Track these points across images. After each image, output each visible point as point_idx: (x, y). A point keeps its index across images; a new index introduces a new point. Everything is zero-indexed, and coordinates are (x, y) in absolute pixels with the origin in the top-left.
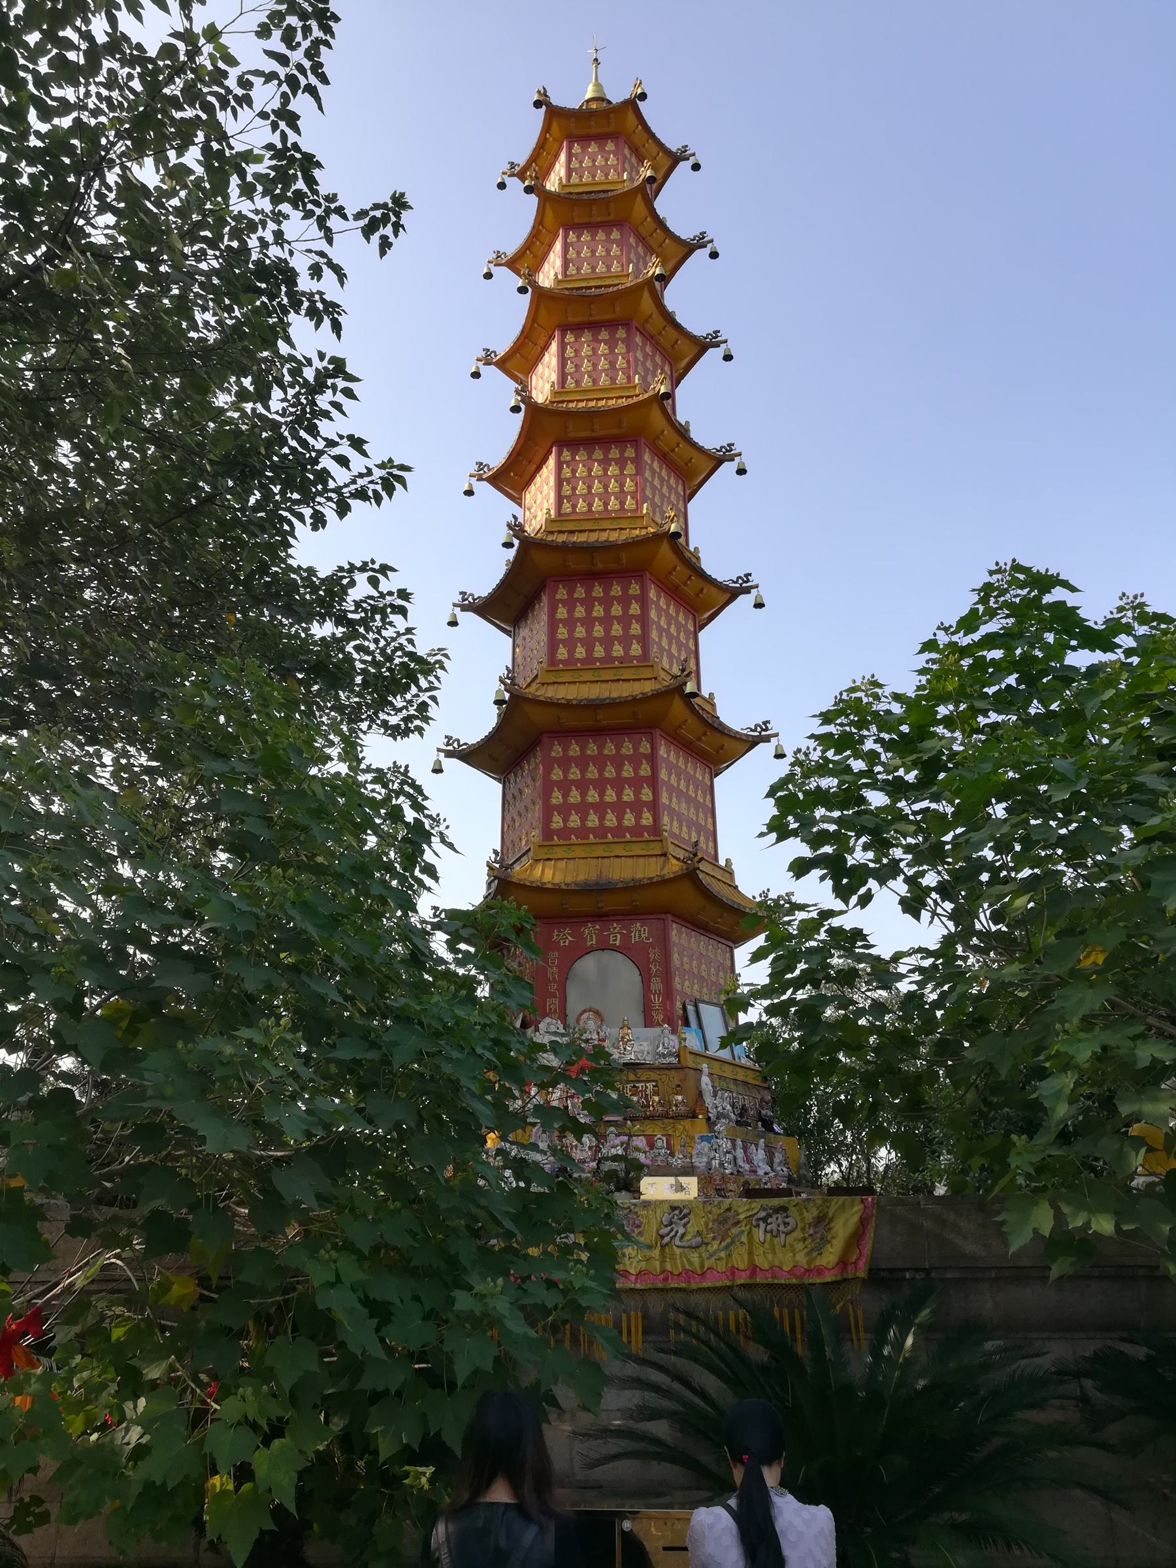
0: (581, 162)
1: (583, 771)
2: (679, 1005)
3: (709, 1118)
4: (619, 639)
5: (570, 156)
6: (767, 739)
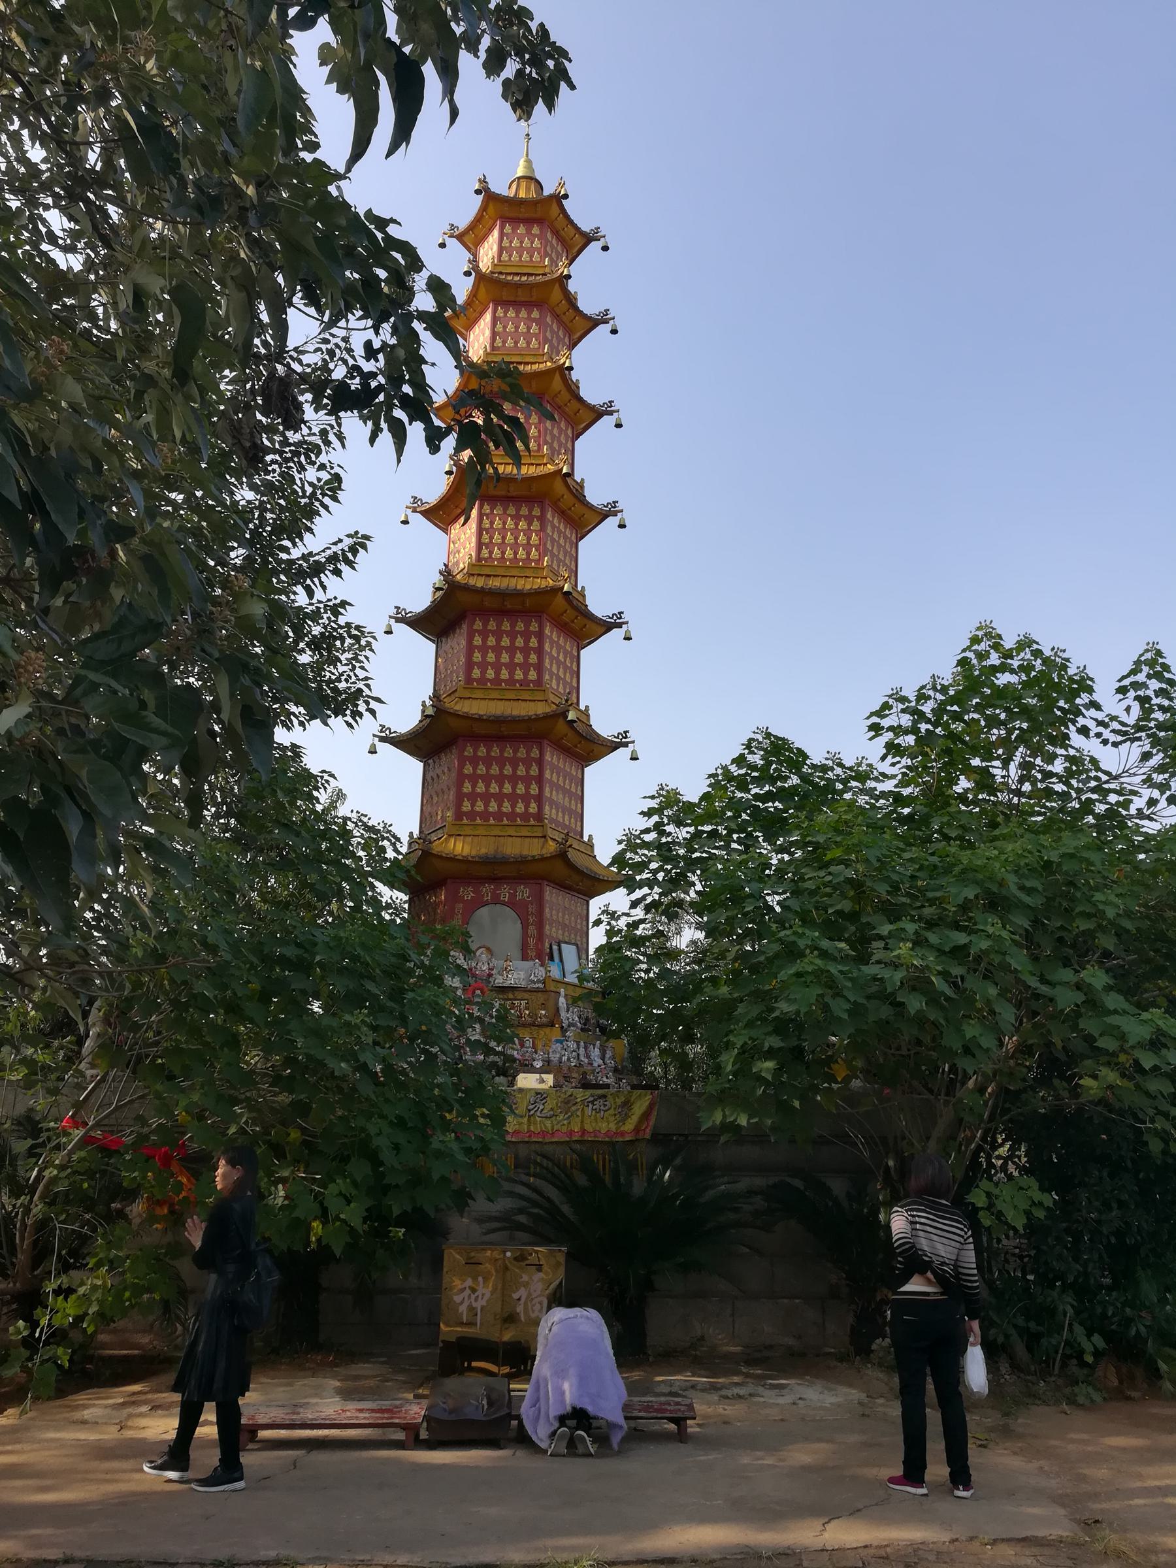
0: (511, 242)
1: (488, 768)
2: (547, 945)
3: (562, 1027)
4: (521, 666)
5: (502, 235)
6: (626, 745)
